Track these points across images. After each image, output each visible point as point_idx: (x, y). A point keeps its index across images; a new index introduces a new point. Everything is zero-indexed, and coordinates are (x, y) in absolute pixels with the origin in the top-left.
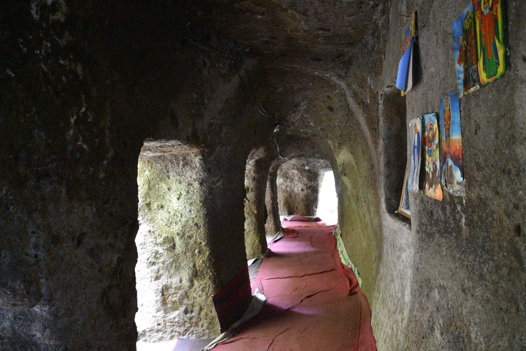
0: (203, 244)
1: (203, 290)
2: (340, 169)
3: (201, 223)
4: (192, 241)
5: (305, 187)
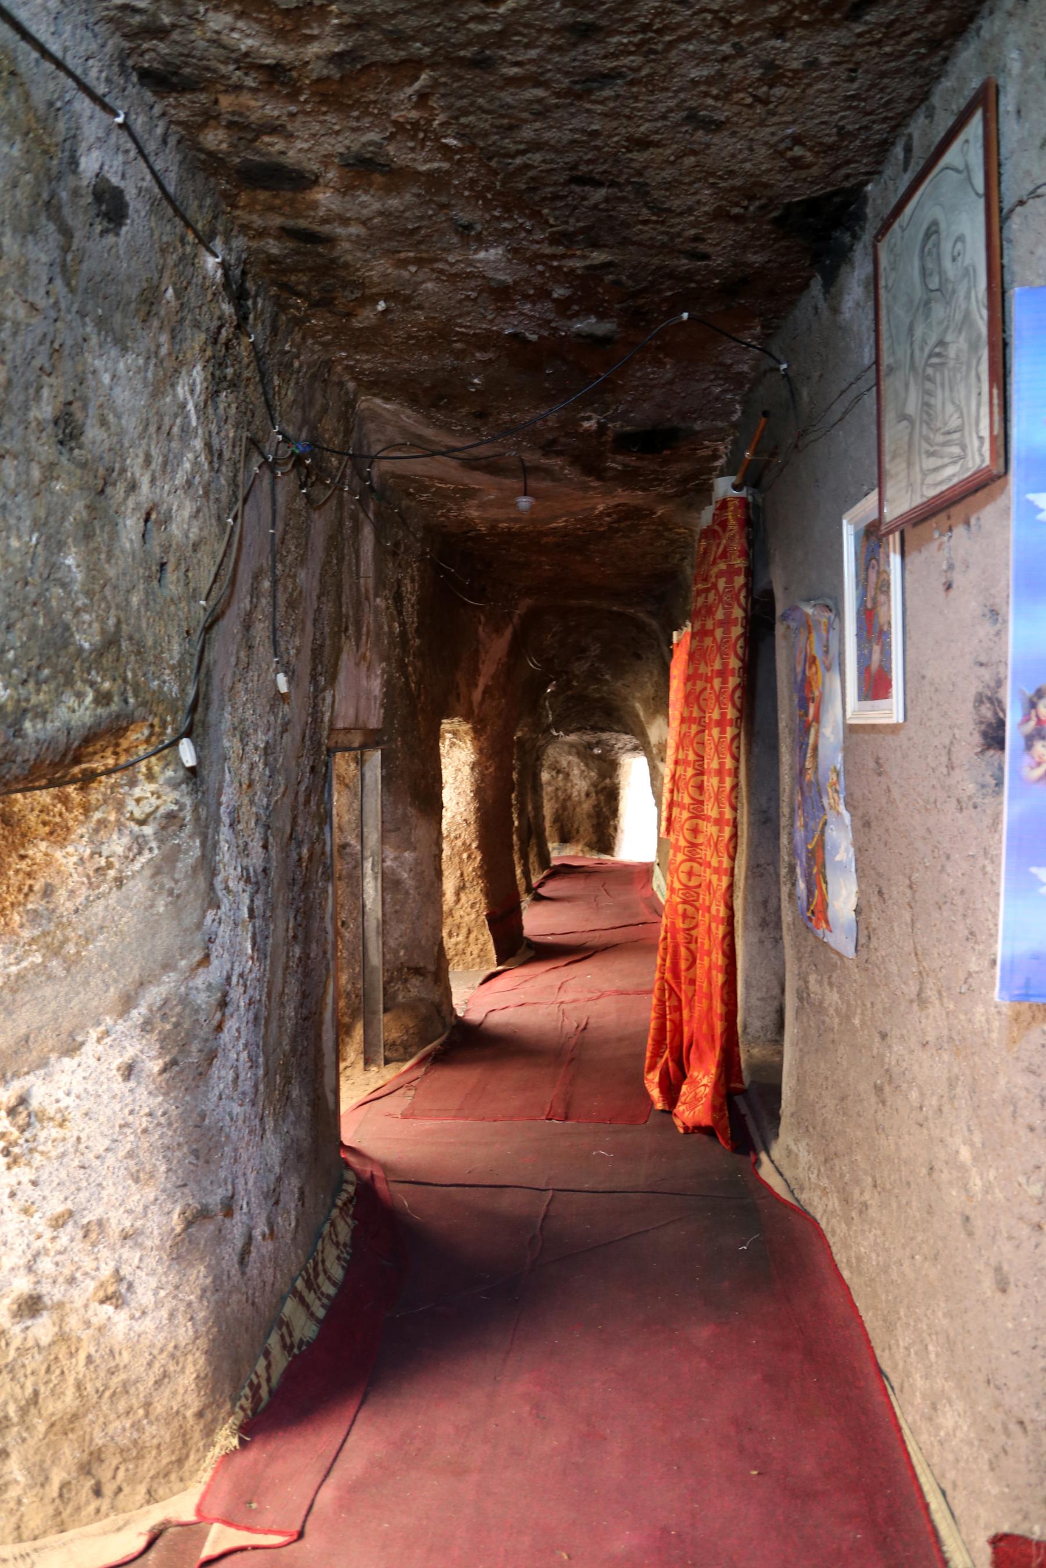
0: (474, 845)
1: (472, 906)
2: (655, 751)
3: (472, 818)
4: (459, 843)
5: (592, 789)
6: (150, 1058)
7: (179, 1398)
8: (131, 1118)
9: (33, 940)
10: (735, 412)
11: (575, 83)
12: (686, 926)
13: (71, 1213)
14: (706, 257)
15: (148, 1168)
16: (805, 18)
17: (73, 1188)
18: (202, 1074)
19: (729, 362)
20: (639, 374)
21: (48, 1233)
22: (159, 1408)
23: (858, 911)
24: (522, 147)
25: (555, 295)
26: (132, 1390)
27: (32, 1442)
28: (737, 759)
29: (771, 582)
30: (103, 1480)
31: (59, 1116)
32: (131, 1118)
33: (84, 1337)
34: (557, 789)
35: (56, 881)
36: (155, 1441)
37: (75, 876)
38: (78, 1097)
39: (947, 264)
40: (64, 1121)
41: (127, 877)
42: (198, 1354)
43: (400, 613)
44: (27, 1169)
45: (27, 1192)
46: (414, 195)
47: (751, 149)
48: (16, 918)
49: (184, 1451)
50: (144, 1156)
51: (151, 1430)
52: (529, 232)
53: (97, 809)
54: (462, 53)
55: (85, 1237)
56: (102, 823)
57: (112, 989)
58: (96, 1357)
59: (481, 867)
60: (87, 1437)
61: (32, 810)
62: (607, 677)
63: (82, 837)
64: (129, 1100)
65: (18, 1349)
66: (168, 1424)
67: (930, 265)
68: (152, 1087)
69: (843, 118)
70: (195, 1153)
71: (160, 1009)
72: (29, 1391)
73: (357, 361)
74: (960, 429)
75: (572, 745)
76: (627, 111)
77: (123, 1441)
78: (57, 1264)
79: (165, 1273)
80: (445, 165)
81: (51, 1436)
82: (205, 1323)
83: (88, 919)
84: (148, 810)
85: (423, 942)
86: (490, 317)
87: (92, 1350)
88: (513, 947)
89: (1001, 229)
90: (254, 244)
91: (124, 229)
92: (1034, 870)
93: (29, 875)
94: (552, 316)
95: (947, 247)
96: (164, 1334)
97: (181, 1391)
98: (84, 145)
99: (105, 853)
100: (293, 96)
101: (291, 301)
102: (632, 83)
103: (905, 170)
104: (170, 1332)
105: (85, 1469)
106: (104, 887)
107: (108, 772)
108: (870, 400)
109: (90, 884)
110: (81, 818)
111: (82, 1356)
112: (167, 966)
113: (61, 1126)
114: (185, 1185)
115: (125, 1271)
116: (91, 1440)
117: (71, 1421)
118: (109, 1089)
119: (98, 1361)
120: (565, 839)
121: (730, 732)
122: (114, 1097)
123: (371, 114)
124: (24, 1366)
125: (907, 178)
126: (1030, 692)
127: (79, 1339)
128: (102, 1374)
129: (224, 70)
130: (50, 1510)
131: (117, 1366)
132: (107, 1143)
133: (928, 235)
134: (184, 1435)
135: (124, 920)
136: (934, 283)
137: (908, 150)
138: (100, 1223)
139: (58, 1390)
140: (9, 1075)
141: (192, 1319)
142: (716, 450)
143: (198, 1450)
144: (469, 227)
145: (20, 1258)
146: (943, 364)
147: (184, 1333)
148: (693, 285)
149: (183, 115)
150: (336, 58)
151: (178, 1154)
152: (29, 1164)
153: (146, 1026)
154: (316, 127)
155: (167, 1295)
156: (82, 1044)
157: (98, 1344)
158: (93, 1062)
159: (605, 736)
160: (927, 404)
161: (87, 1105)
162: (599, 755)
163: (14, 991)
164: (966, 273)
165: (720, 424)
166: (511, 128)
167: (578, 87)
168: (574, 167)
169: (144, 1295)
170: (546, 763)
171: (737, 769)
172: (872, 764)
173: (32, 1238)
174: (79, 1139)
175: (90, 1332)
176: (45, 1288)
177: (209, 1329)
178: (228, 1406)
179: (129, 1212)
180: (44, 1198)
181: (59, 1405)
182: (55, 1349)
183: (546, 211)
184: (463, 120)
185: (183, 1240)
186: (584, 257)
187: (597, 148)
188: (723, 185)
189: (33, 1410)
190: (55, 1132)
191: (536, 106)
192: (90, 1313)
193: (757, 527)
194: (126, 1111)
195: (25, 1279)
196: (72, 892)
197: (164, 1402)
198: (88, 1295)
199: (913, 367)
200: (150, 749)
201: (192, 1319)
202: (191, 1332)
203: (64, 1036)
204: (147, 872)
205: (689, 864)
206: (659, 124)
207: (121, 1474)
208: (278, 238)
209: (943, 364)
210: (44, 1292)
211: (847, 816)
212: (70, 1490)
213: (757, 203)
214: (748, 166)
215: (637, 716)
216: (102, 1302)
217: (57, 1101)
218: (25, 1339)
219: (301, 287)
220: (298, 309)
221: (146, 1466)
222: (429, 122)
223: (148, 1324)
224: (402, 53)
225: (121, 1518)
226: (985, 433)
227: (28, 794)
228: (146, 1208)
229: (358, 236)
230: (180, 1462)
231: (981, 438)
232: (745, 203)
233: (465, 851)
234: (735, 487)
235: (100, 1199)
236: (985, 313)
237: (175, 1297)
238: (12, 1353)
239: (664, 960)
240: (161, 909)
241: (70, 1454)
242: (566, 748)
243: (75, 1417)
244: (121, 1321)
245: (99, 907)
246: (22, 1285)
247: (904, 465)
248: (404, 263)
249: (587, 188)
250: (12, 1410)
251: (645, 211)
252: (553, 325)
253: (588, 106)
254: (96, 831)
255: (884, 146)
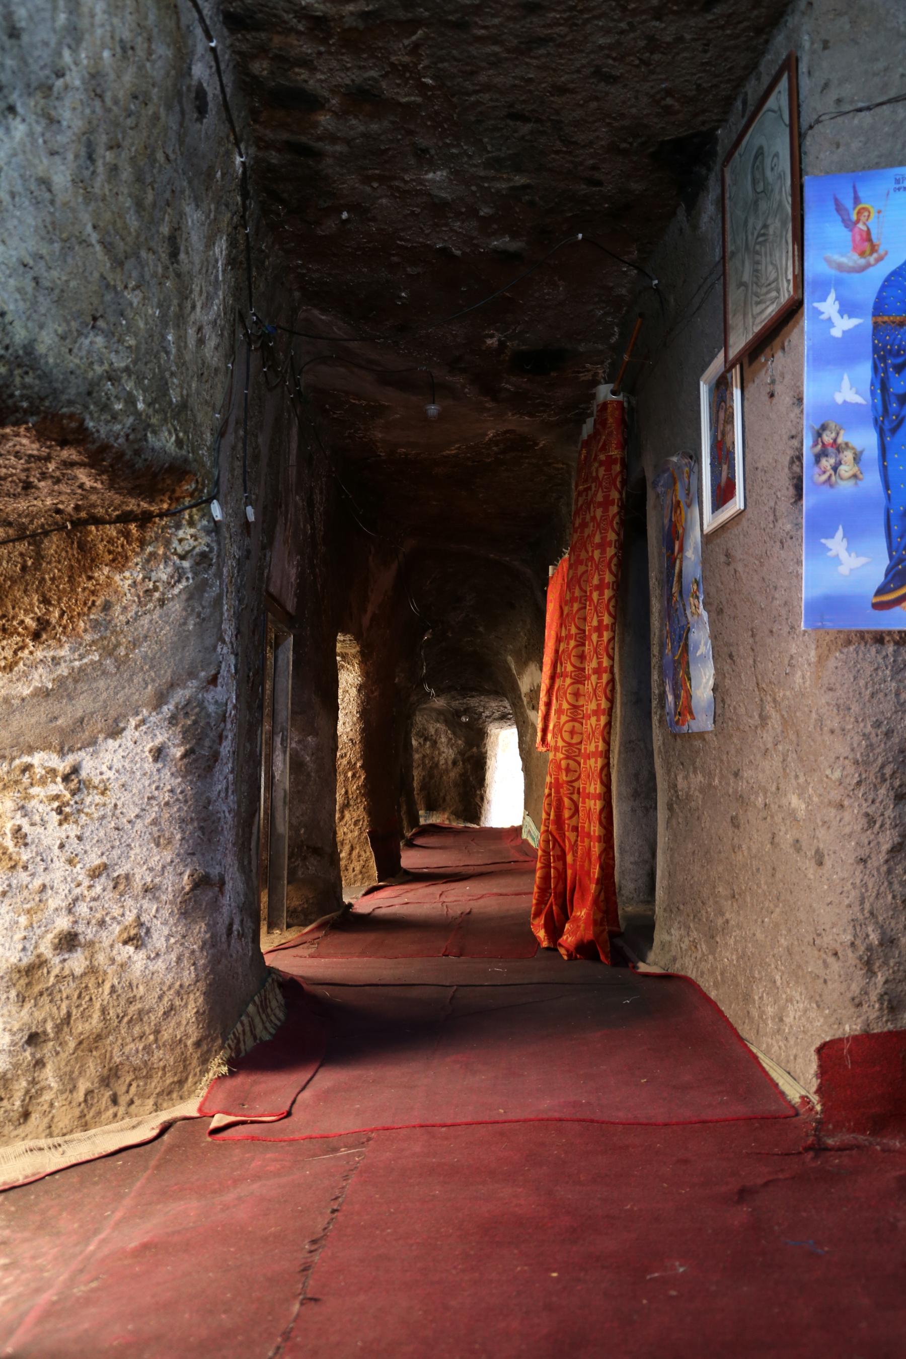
0: (359, 764)
1: (356, 824)
3: (358, 739)
6: (175, 746)
7: (182, 1029)
8: (156, 793)
9: (93, 642)
10: (613, 335)
11: (522, 43)
12: (569, 779)
13: (105, 866)
14: (599, 183)
15: (167, 835)
16: (675, 8)
17: (108, 846)
18: (210, 769)
19: (611, 284)
20: (537, 294)
21: (86, 883)
22: (166, 1036)
23: (714, 690)
24: (477, 88)
25: (482, 214)
26: (145, 1019)
27: (63, 1056)
28: (611, 658)
29: (643, 471)
30: (119, 1093)
31: (102, 785)
32: (156, 793)
33: (109, 971)
34: (424, 756)
35: (114, 599)
36: (161, 1064)
37: (129, 595)
38: (118, 771)
39: (768, 173)
40: (106, 789)
41: (168, 599)
42: (198, 994)
43: (312, 517)
44: (74, 826)
45: (74, 845)
46: (393, 123)
47: (636, 98)
48: (82, 624)
49: (184, 1075)
50: (165, 825)
51: (158, 1054)
52: (470, 157)
53: (150, 544)
54: (450, 18)
55: (114, 888)
56: (153, 555)
57: (150, 687)
58: (119, 987)
59: (364, 786)
60: (108, 1055)
61: (102, 540)
62: (481, 629)
63: (137, 564)
64: (156, 778)
65: (57, 976)
66: (172, 1050)
67: (758, 176)
68: (174, 769)
69: (700, 78)
70: (201, 828)
71: (183, 708)
72: (64, 1011)
73: (309, 269)
74: (776, 279)
75: (440, 712)
76: (554, 65)
77: (136, 1061)
78: (91, 909)
79: (175, 924)
80: (419, 99)
81: (79, 1052)
82: (204, 970)
83: (136, 629)
84: (187, 548)
85: (322, 823)
86: (427, 232)
87: (116, 982)
88: (391, 872)
89: (800, 146)
90: (260, 154)
91: (205, 121)
92: (823, 541)
93: (93, 593)
94: (475, 233)
95: (768, 162)
96: (172, 974)
97: (184, 1022)
98: (196, 57)
99: (153, 579)
100: (324, 41)
101: (273, 207)
102: (559, 46)
103: (743, 117)
104: (177, 973)
105: (105, 1081)
106: (150, 606)
107: (161, 515)
108: (719, 287)
109: (140, 602)
110: (138, 550)
111: (107, 987)
112: (192, 675)
113: (103, 793)
114: (193, 854)
115: (145, 918)
116: (111, 1058)
117: (96, 1041)
118: (141, 768)
119: (120, 991)
120: (431, 807)
121: (606, 635)
122: (145, 774)
123: (377, 57)
124: (60, 991)
125: (744, 121)
126: (817, 427)
127: (105, 973)
128: (123, 1003)
129: (286, 17)
130: (77, 1112)
131: (135, 996)
132: (137, 811)
133: (756, 157)
134: (185, 1061)
135: (164, 632)
136: (760, 188)
137: (745, 103)
138: (127, 877)
139: (87, 1013)
140: (66, 748)
141: (194, 964)
142: (596, 374)
143: (195, 1075)
144: (425, 151)
145: (63, 901)
146: (765, 241)
147: (188, 976)
148: (588, 208)
149: (244, 47)
150: (364, 15)
151: (190, 827)
152: (76, 822)
153: (173, 720)
154: (334, 64)
155: (175, 943)
156: (124, 729)
157: (120, 977)
158: (130, 744)
159: (473, 702)
160: (756, 271)
161: (124, 779)
162: (466, 723)
163: (76, 681)
164: (780, 177)
165: (600, 347)
166: (472, 73)
167: (523, 46)
168: (511, 106)
169: (158, 940)
170: (414, 732)
171: (612, 666)
172: (722, 559)
173: (73, 885)
174: (116, 805)
175: (114, 967)
176: (80, 928)
177: (208, 975)
178: (220, 1041)
179: (151, 869)
180: (86, 852)
181: (87, 1026)
182: (86, 980)
183: (486, 140)
184: (440, 65)
185: (190, 899)
186: (509, 180)
187: (530, 91)
188: (616, 124)
189: (66, 1029)
190: (98, 799)
191: (492, 58)
192: (115, 952)
193: (633, 428)
194: (153, 787)
195: (66, 919)
196: (125, 609)
197: (171, 1031)
198: (113, 937)
199: (747, 248)
200: (193, 502)
201: (194, 964)
202: (193, 975)
203: (110, 722)
204: (184, 597)
205: (571, 724)
206: (575, 76)
207: (133, 1089)
208: (279, 150)
209: (765, 241)
210: (80, 931)
211: (705, 615)
212: (93, 1098)
213: (639, 140)
214: (634, 110)
215: (510, 669)
216: (125, 943)
217: (101, 774)
218: (63, 969)
219: (285, 195)
220: (278, 215)
221: (153, 1084)
222: (416, 65)
223: (160, 965)
224: (410, 15)
225: (134, 1121)
226: (790, 277)
227: (101, 527)
228: (164, 867)
229: (341, 153)
230: (181, 1083)
231: (788, 281)
232: (631, 140)
233: (350, 769)
234: (614, 393)
235: (128, 857)
236: (790, 199)
237: (182, 944)
238: (52, 980)
239: (549, 815)
240: (191, 627)
241: (93, 1068)
242: (434, 715)
243: (99, 1037)
244: (139, 959)
245: (145, 621)
246: (63, 923)
247: (741, 317)
248: (367, 180)
249: (518, 123)
250: (49, 1027)
251: (558, 142)
252: (475, 242)
253: (527, 60)
254: (148, 561)
255: (729, 101)
